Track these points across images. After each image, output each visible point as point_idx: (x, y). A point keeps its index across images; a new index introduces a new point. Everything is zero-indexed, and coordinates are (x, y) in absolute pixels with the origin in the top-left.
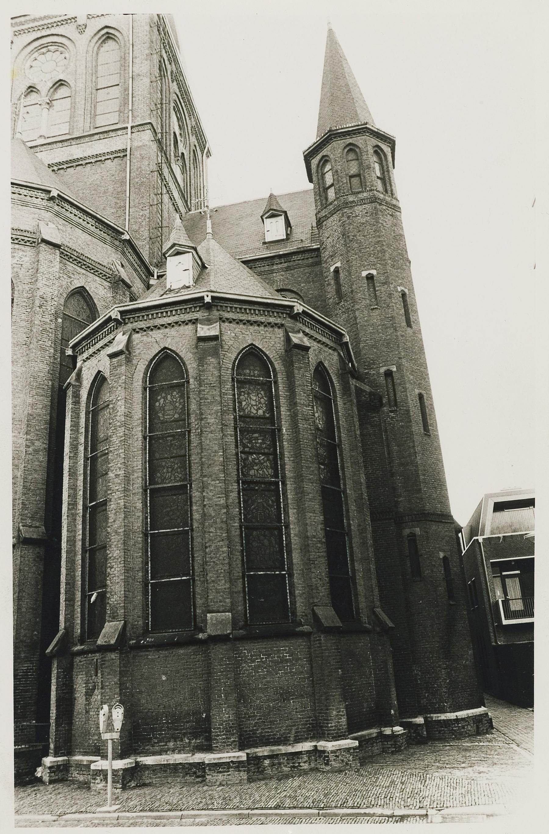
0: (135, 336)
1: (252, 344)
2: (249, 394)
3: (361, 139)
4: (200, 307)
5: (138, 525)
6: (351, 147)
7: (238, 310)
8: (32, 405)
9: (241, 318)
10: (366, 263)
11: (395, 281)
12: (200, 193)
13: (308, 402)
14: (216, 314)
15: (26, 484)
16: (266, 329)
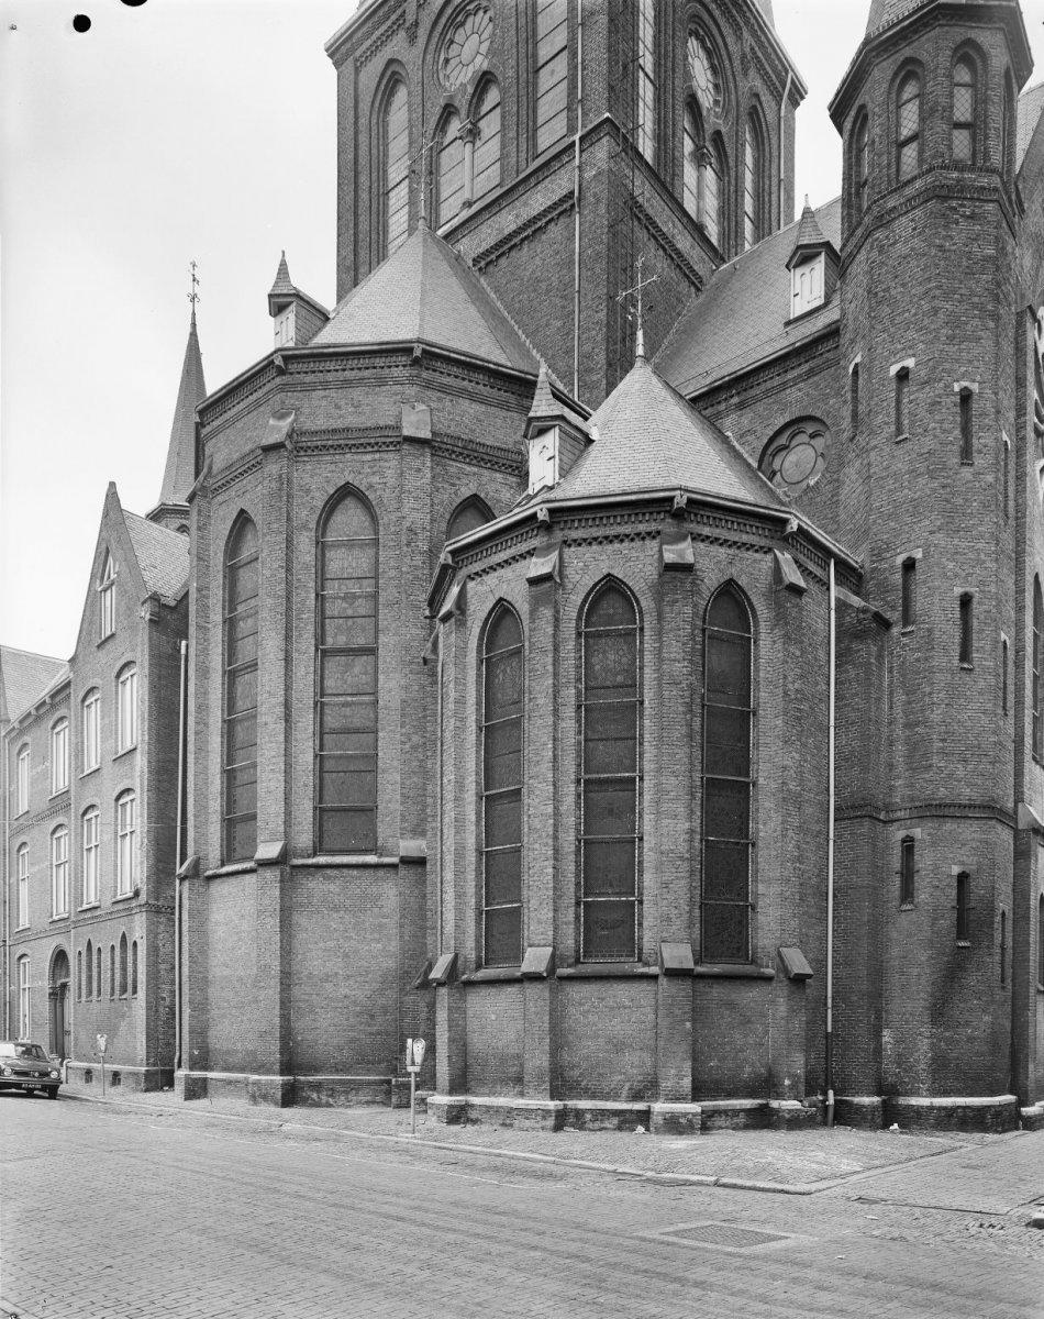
0: (471, 585)
1: (609, 575)
2: (604, 652)
3: (928, 40)
4: (538, 528)
5: (471, 842)
6: (909, 68)
7: (590, 523)
8: (406, 688)
9: (595, 535)
10: (899, 347)
11: (949, 372)
12: (770, 201)
13: (683, 654)
14: (558, 535)
15: (404, 791)
16: (633, 544)
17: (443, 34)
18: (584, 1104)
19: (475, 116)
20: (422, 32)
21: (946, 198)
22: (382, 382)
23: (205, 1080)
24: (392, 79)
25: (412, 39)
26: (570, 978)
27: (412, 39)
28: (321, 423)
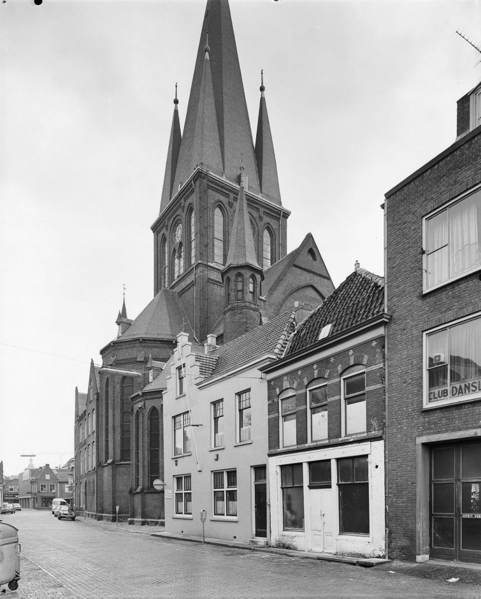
14: (144, 398)
17: (174, 228)
18: (149, 520)
19: (180, 253)
20: (169, 228)
21: (233, 310)
22: (134, 347)
23: (102, 516)
24: (164, 239)
25: (167, 229)
26: (147, 493)
27: (167, 229)
28: (121, 358)
